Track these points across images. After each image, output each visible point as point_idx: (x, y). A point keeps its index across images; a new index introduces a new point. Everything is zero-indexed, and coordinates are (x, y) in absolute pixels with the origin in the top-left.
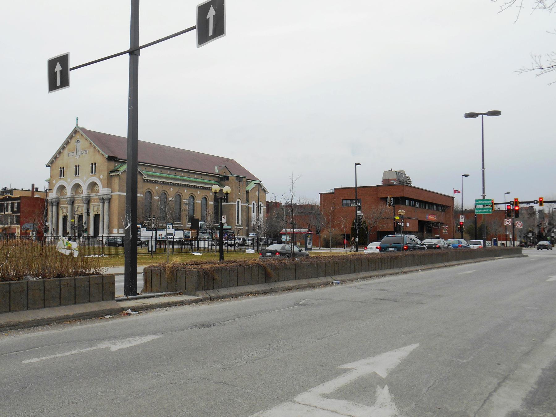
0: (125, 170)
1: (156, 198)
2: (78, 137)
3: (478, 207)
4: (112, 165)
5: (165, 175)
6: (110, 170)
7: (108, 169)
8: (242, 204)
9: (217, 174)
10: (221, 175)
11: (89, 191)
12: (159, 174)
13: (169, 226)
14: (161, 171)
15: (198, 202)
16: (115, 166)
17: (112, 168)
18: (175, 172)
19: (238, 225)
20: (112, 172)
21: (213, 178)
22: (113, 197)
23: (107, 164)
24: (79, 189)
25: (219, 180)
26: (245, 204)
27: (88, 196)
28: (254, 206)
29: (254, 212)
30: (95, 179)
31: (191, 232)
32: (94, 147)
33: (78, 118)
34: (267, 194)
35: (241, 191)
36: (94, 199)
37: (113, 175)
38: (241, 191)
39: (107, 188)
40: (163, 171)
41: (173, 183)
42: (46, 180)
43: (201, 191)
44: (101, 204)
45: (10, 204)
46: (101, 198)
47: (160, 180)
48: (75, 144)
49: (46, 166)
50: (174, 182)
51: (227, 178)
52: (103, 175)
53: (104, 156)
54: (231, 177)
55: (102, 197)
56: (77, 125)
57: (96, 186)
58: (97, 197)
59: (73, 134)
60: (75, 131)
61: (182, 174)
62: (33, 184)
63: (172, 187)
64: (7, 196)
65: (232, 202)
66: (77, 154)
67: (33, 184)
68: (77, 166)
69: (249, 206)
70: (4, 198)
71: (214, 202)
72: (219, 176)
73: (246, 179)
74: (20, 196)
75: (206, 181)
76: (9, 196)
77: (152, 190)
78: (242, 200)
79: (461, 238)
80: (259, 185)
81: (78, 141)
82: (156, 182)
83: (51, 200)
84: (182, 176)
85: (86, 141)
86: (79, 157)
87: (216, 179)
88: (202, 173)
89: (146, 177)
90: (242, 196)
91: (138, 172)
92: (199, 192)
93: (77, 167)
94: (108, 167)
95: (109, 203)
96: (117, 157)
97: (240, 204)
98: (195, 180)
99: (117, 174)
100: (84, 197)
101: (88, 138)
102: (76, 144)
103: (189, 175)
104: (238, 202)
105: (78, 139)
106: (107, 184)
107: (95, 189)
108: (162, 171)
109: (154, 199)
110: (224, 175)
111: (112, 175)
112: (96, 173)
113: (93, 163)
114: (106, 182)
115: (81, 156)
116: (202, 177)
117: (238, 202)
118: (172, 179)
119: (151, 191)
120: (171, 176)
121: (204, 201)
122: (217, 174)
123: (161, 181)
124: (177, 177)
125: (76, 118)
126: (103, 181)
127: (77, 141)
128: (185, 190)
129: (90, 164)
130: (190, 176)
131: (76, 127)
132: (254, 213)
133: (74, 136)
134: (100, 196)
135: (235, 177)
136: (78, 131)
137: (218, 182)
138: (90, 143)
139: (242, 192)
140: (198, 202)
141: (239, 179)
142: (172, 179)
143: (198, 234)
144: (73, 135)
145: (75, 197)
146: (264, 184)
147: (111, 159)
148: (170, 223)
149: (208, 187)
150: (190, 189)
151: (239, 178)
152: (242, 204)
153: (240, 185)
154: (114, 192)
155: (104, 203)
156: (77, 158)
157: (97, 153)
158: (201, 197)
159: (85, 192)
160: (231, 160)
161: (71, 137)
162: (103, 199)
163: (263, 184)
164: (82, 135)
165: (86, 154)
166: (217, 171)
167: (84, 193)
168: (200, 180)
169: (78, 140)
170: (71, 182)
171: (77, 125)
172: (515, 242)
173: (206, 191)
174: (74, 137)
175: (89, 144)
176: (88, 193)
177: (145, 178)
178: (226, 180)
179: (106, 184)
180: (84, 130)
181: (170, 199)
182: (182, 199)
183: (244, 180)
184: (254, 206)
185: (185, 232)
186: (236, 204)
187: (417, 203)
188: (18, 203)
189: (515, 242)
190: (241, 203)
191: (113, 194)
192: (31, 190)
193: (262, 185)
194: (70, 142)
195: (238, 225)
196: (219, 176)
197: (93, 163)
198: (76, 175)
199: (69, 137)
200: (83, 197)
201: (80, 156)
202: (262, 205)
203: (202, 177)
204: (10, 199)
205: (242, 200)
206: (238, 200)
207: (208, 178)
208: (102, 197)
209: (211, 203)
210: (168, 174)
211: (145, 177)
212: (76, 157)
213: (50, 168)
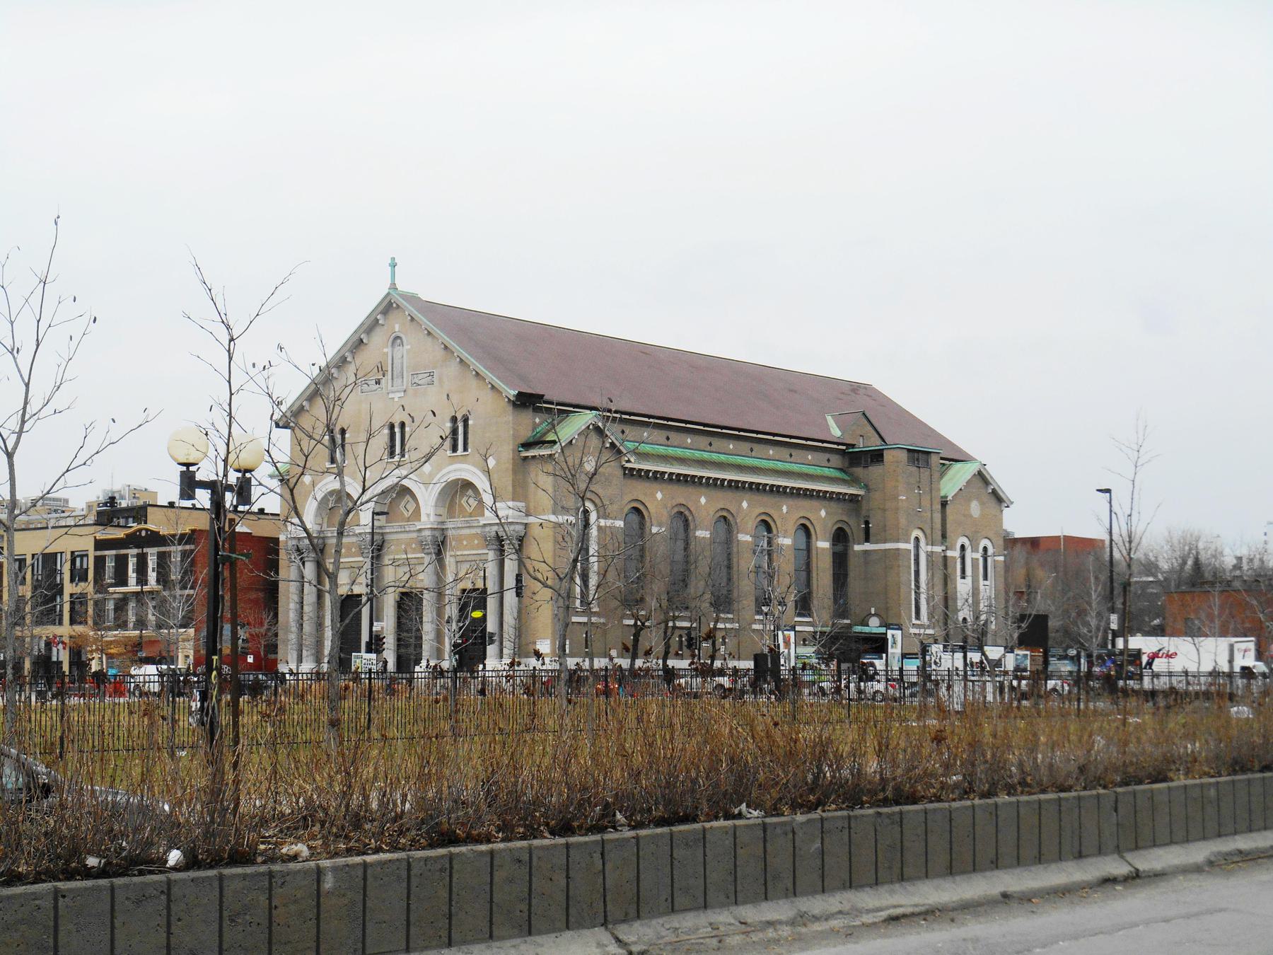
0: (571, 441)
1: (703, 534)
2: (396, 325)
4: (530, 423)
5: (679, 452)
6: (522, 441)
7: (515, 437)
8: (929, 548)
9: (838, 444)
10: (853, 446)
11: (441, 511)
12: (661, 450)
13: (893, 636)
14: (668, 438)
15: (786, 541)
16: (535, 426)
17: (526, 434)
18: (710, 439)
19: (918, 622)
20: (527, 445)
21: (827, 456)
22: (536, 531)
23: (511, 418)
24: (403, 504)
25: (847, 464)
26: (938, 549)
27: (439, 527)
28: (917, 547)
29: (986, 578)
30: (468, 471)
31: (1031, 656)
32: (461, 360)
34: (1006, 511)
35: (926, 502)
36: (459, 539)
37: (534, 457)
38: (926, 502)
39: (513, 500)
40: (718, 443)
41: (709, 478)
43: (791, 502)
44: (491, 555)
45: (133, 556)
46: (493, 534)
47: (668, 469)
48: (385, 350)
50: (710, 475)
51: (877, 457)
52: (501, 459)
53: (500, 392)
54: (889, 451)
55: (497, 532)
56: (393, 286)
58: (479, 530)
59: (378, 317)
60: (388, 307)
61: (689, 441)
63: (703, 490)
64: (140, 530)
65: (898, 541)
68: (397, 425)
69: (949, 553)
70: (127, 535)
71: (833, 540)
72: (844, 448)
73: (942, 459)
74: (193, 531)
75: (805, 469)
76: (147, 530)
77: (643, 504)
78: (928, 532)
79: (905, 651)
80: (982, 477)
81: (399, 341)
82: (657, 477)
83: (294, 542)
84: (730, 451)
85: (429, 339)
86: (402, 394)
87: (836, 460)
88: (742, 433)
89: (632, 460)
90: (929, 521)
91: (608, 445)
92: (785, 509)
93: (397, 430)
94: (514, 429)
95: (519, 551)
96: (543, 396)
97: (925, 548)
98: (771, 464)
99: (545, 452)
100: (427, 533)
101: (436, 331)
102: (388, 350)
103: (752, 450)
104: (917, 539)
106: (514, 486)
107: (465, 504)
108: (627, 432)
109: (854, 551)
110: (861, 445)
111: (526, 458)
112: (469, 450)
115: (410, 392)
116: (791, 455)
117: (917, 539)
118: (702, 463)
119: (641, 507)
120: (698, 454)
121: (803, 539)
122: (838, 444)
123: (671, 474)
124: (715, 457)
128: (820, 510)
129: (449, 418)
130: (754, 454)
131: (388, 294)
132: (963, 577)
133: (380, 322)
134: (487, 529)
135: (905, 451)
136: (398, 306)
137: (841, 470)
138: (446, 348)
139: (929, 505)
140: (786, 541)
141: (918, 460)
142: (702, 463)
143: (1046, 663)
144: (378, 320)
145: (388, 531)
146: (1002, 479)
147: (526, 401)
148: (896, 625)
149: (814, 487)
150: (719, 494)
151: (918, 457)
152: (929, 548)
153: (922, 480)
155: (501, 551)
156: (396, 399)
157: (474, 382)
158: (791, 526)
159: (428, 515)
160: (866, 388)
161: (371, 325)
162: (499, 540)
163: (994, 472)
164: (412, 319)
166: (836, 432)
167: (424, 518)
168: (788, 467)
169: (398, 337)
171: (393, 286)
172: (1049, 682)
173: (806, 503)
175: (440, 353)
176: (440, 519)
177: (628, 465)
178: (872, 461)
179: (510, 488)
180: (413, 299)
181: (654, 530)
182: (648, 524)
183: (935, 460)
184: (917, 547)
185: (1017, 655)
186: (911, 546)
188: (185, 554)
189: (1049, 682)
190: (927, 544)
191: (531, 520)
192: (209, 507)
193: (991, 477)
195: (918, 622)
196: (844, 448)
197: (459, 417)
198: (392, 454)
199: (366, 326)
200: (420, 530)
201: (405, 391)
202: (990, 551)
203: (791, 455)
204: (155, 539)
205: (928, 532)
206: (984, 542)
207: (810, 457)
208: (497, 532)
209: (823, 545)
210: (689, 446)
211: (628, 461)
212: (391, 396)
213: (289, 430)
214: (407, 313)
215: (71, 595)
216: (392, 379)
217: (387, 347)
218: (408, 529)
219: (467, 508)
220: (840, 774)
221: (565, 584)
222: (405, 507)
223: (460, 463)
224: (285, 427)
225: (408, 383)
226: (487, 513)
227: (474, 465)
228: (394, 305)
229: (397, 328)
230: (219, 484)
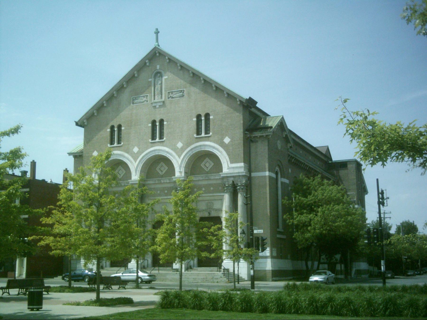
3: (57, 231)
33: (159, 30)
42: (69, 151)
48: (150, 80)
49: (77, 124)
57: (205, 161)
62: (33, 161)
66: (154, 99)
67: (33, 161)
81: (159, 75)
105: (159, 71)
113: (116, 126)
114: (240, 151)
125: (155, 30)
126: (231, 148)
127: (153, 75)
129: (195, 115)
154: (255, 172)
165: (183, 96)
170: (139, 153)
174: (148, 66)
187: (288, 214)
194: (136, 77)
197: (116, 126)
198: (153, 138)
208: (233, 182)
214: (167, 58)
215: (220, 271)
216: (154, 96)
217: (151, 78)
218: (162, 182)
219: (205, 169)
220: (281, 302)
221: (40, 234)
222: (162, 169)
223: (203, 141)
224: (81, 126)
225: (165, 96)
226: (355, 130)
227: (214, 142)
228: (158, 55)
229: (158, 67)
230: (40, 307)
